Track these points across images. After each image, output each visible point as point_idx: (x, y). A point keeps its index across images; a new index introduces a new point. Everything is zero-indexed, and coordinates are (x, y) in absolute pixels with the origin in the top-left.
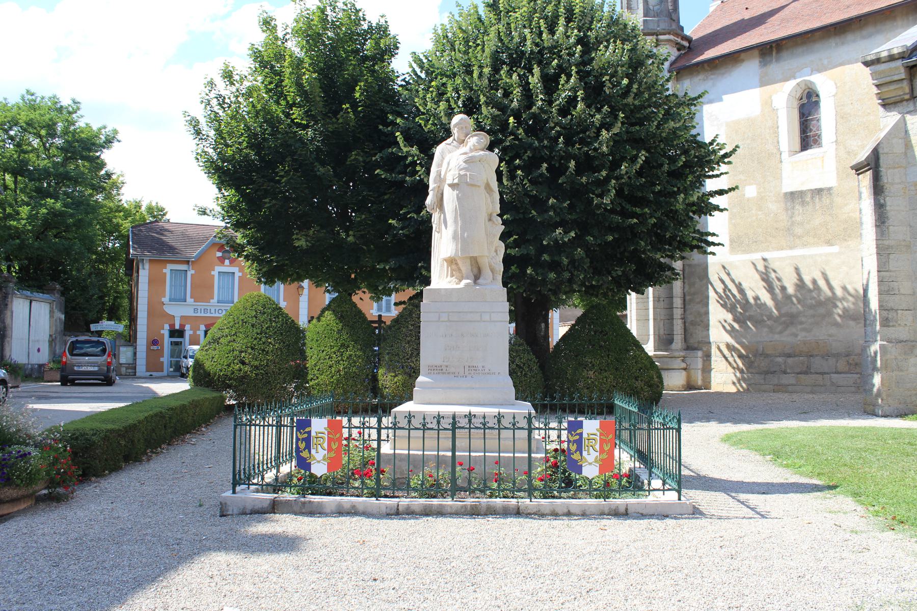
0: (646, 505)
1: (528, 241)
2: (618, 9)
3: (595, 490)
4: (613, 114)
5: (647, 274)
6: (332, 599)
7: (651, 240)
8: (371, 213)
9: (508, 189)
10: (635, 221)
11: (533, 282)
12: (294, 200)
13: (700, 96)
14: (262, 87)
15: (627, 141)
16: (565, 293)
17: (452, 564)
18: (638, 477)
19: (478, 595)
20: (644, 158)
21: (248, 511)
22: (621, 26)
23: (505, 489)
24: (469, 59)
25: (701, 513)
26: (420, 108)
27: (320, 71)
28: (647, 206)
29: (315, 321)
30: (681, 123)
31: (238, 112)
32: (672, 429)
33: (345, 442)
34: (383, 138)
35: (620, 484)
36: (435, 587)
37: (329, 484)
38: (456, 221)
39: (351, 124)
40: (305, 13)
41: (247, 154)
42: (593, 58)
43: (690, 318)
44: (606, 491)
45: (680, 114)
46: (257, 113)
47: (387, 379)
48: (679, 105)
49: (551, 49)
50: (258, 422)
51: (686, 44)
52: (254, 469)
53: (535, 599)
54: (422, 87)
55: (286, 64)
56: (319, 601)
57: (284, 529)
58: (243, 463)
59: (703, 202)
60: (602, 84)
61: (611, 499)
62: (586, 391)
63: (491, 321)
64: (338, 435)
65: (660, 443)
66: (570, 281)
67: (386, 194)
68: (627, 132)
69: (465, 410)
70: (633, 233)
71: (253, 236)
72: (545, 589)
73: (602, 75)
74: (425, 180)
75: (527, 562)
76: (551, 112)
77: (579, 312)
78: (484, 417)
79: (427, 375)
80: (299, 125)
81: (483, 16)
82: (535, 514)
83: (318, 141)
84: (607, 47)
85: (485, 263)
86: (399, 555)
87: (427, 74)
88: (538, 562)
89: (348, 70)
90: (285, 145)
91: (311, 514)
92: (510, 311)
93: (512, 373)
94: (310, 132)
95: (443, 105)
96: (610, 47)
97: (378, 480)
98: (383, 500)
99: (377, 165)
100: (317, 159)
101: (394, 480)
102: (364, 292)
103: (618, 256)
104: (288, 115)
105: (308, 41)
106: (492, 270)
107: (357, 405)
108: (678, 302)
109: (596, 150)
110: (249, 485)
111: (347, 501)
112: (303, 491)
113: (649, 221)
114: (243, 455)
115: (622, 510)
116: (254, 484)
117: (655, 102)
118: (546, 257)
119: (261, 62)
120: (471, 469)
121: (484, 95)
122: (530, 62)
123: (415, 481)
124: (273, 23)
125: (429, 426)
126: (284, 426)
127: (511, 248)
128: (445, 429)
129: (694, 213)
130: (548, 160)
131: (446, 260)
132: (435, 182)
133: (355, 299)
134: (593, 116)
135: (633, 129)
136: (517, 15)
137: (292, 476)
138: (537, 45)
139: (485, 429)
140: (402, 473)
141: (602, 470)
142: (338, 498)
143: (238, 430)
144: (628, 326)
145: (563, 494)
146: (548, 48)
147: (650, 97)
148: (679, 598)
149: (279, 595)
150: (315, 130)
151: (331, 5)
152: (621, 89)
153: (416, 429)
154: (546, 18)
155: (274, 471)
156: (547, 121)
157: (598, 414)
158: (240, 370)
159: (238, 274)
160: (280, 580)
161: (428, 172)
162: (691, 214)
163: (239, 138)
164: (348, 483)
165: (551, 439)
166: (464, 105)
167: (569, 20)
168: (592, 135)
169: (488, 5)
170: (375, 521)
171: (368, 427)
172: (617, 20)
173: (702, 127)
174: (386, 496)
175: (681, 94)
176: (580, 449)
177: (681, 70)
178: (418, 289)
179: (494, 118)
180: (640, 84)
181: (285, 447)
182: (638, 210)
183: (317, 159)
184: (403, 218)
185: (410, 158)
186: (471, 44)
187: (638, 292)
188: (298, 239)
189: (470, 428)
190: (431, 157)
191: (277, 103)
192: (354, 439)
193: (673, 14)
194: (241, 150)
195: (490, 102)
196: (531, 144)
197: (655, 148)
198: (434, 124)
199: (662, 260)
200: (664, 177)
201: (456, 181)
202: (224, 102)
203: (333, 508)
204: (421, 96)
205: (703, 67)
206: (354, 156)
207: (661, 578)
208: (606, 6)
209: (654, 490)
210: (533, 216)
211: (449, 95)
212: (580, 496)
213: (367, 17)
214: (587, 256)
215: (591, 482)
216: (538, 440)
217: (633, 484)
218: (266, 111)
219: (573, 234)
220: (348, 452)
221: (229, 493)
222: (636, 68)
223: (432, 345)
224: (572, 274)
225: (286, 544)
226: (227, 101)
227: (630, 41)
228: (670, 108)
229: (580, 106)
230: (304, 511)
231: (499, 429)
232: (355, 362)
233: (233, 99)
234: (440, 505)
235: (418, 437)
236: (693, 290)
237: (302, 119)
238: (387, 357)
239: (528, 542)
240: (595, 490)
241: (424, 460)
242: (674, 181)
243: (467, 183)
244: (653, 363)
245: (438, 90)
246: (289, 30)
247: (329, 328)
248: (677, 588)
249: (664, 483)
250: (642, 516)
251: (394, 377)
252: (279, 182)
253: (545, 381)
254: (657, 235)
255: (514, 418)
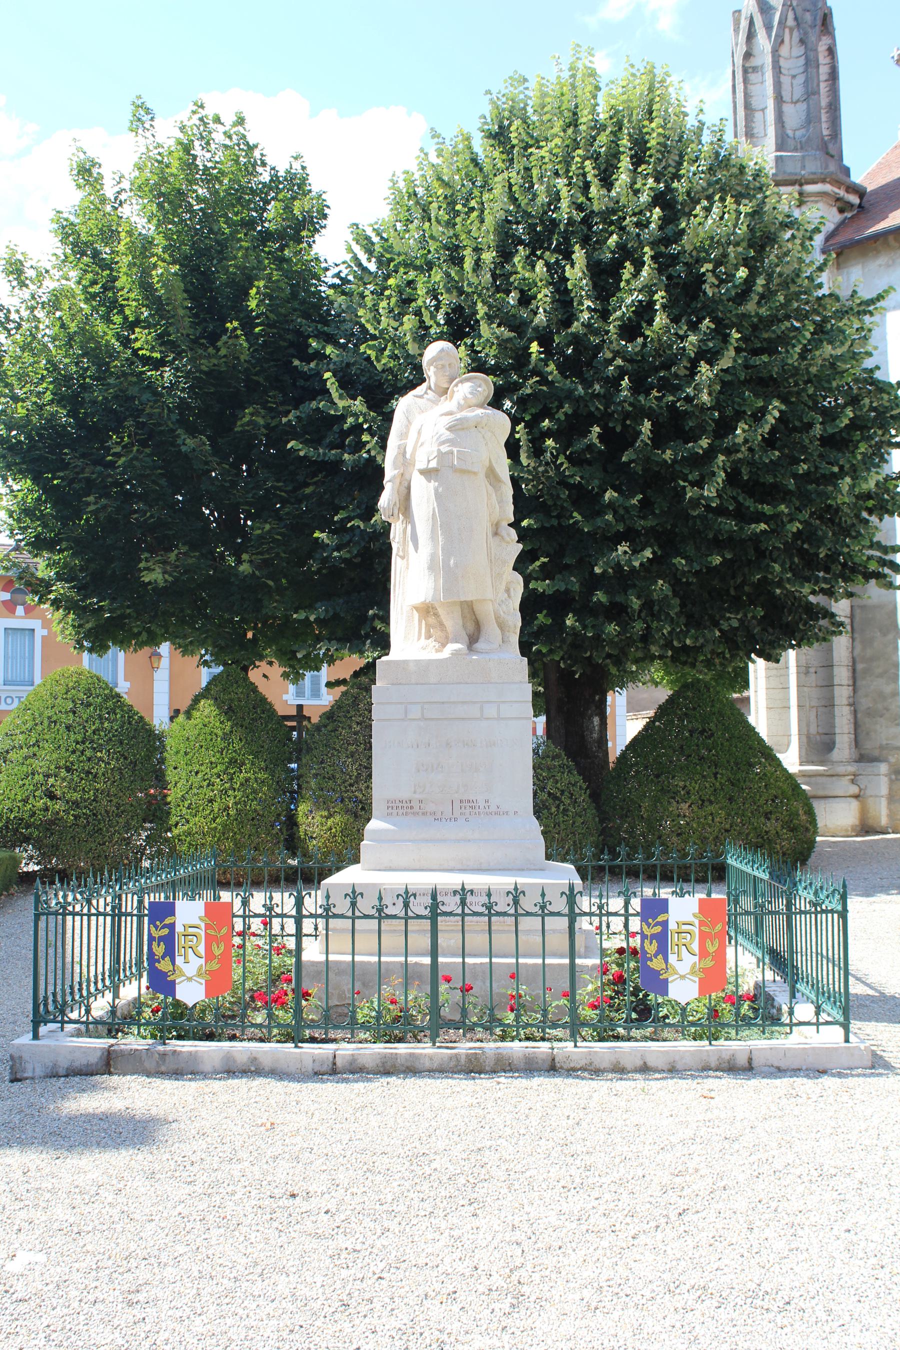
0: (786, 1052)
1: (567, 567)
2: (729, 137)
3: (693, 1024)
4: (721, 332)
5: (785, 625)
6: (215, 1232)
7: (792, 563)
8: (280, 519)
9: (529, 472)
10: (763, 526)
11: (577, 642)
12: (139, 497)
13: (880, 297)
14: (78, 290)
15: (747, 382)
16: (636, 661)
17: (434, 1165)
18: (770, 999)
19: (480, 1222)
20: (777, 414)
21: (62, 1072)
22: (735, 170)
23: (527, 1025)
24: (456, 236)
25: (887, 1066)
26: (368, 326)
27: (183, 261)
28: (783, 501)
29: (181, 718)
30: (845, 348)
31: (34, 337)
32: (832, 911)
33: (237, 941)
34: (301, 383)
35: (737, 1014)
36: (402, 1208)
37: (209, 1018)
38: (433, 537)
39: (242, 358)
40: (154, 153)
41: (53, 415)
42: (683, 231)
43: (865, 703)
44: (711, 1026)
45: (843, 332)
46: (71, 338)
47: (313, 822)
48: (843, 313)
49: (606, 215)
50: (78, 908)
51: (854, 199)
52: (72, 993)
53: (584, 1228)
54: (371, 287)
55: (121, 248)
56: (191, 1237)
57: (127, 1103)
58: (51, 980)
59: (887, 491)
60: (700, 279)
61: (722, 1042)
62: (675, 839)
63: (499, 718)
64: (224, 931)
65: (810, 937)
66: (646, 638)
67: (307, 485)
68: (746, 367)
69: (454, 880)
70: (757, 552)
71: (66, 565)
72: (601, 1210)
73: (699, 261)
74: (379, 459)
75: (570, 1160)
76: (607, 332)
77: (663, 694)
78: (489, 895)
79: (385, 818)
80: (146, 360)
81: (481, 155)
82: (583, 1069)
83: (183, 390)
84: (708, 210)
85: (487, 612)
86: (337, 1149)
87: (380, 263)
88: (589, 1160)
89: (235, 258)
90: (123, 398)
91: (177, 1074)
92: (535, 694)
93: (538, 811)
94: (168, 374)
95: (409, 322)
96: (715, 210)
97: (298, 1012)
98: (309, 1048)
99: (291, 432)
100: (182, 422)
101: (328, 1009)
102: (271, 663)
103: (732, 592)
104: (126, 342)
105: (160, 206)
106: (502, 626)
107: (261, 869)
108: (842, 675)
109: (688, 399)
110: (63, 1022)
111: (242, 1049)
112: (161, 1033)
113: (788, 526)
114: (51, 967)
115: (742, 1061)
116: (71, 1021)
117: (798, 309)
118: (600, 596)
119: (75, 245)
120: (466, 989)
121: (484, 302)
122: (567, 240)
123: (366, 1011)
124: (95, 171)
125: (388, 911)
126: (127, 914)
127: (536, 579)
128: (419, 917)
129: (870, 511)
130: (603, 419)
131: (416, 608)
132: (395, 466)
133: (254, 675)
134: (683, 338)
135: (757, 360)
136: (543, 152)
137: (142, 1004)
138: (580, 208)
139: (490, 915)
140: (341, 996)
141: (704, 988)
142: (226, 1045)
143: (42, 924)
144: (752, 720)
145: (635, 1033)
146: (600, 213)
147: (788, 300)
148: (847, 1225)
149: (119, 1227)
150: (177, 369)
151: (202, 138)
152: (735, 286)
153: (366, 917)
154: (596, 157)
155: (109, 996)
156: (599, 348)
157: (697, 881)
158: (46, 809)
159: (40, 633)
160: (121, 1199)
161: (383, 446)
162: (865, 514)
163: (37, 384)
164: (244, 1015)
165: (613, 928)
166: (449, 321)
167: (638, 160)
168: (683, 372)
169: (490, 135)
170: (294, 1086)
171: (278, 916)
172: (727, 158)
173: (885, 353)
174: (313, 1040)
175: (844, 294)
176: (663, 950)
177: (845, 248)
178: (370, 655)
179: (503, 344)
180: (769, 277)
181: (129, 953)
182: (767, 509)
183: (182, 422)
184: (339, 530)
185: (350, 420)
186: (459, 207)
187: (768, 658)
188: (147, 569)
189: (463, 915)
190: (388, 418)
191: (108, 320)
192: (254, 935)
193: (829, 145)
194: (41, 407)
195: (497, 315)
196: (571, 392)
197: (798, 394)
198: (394, 357)
199: (812, 598)
200: (815, 448)
201: (433, 464)
202: (8, 320)
203: (217, 1063)
204: (369, 304)
205: (886, 244)
206: (250, 417)
207: (814, 1187)
208: (706, 132)
209: (800, 1024)
210: (576, 523)
211: (420, 302)
212: (665, 1034)
213: (267, 160)
214: (675, 594)
215: (684, 1009)
216: (587, 932)
217: (763, 1012)
218: (86, 334)
219: (648, 553)
220: (242, 960)
221: (26, 1039)
222: (762, 248)
223: (393, 766)
224: (648, 628)
225: (132, 1132)
226: (14, 316)
227: (750, 198)
228: (825, 320)
229: (660, 320)
230: (163, 1069)
231: (516, 915)
232: (255, 792)
233: (25, 314)
234: (411, 1054)
235: (370, 931)
236: (869, 652)
237: (152, 350)
238: (313, 783)
239: (571, 1122)
240: (693, 1024)
241: (380, 973)
242: (833, 455)
243: (452, 466)
244: (796, 787)
245: (400, 293)
246: (126, 185)
247: (207, 730)
248: (844, 1206)
249: (818, 1010)
250: (779, 1071)
251: (327, 818)
252: (112, 465)
253: (602, 821)
254: (802, 553)
255: (543, 895)
